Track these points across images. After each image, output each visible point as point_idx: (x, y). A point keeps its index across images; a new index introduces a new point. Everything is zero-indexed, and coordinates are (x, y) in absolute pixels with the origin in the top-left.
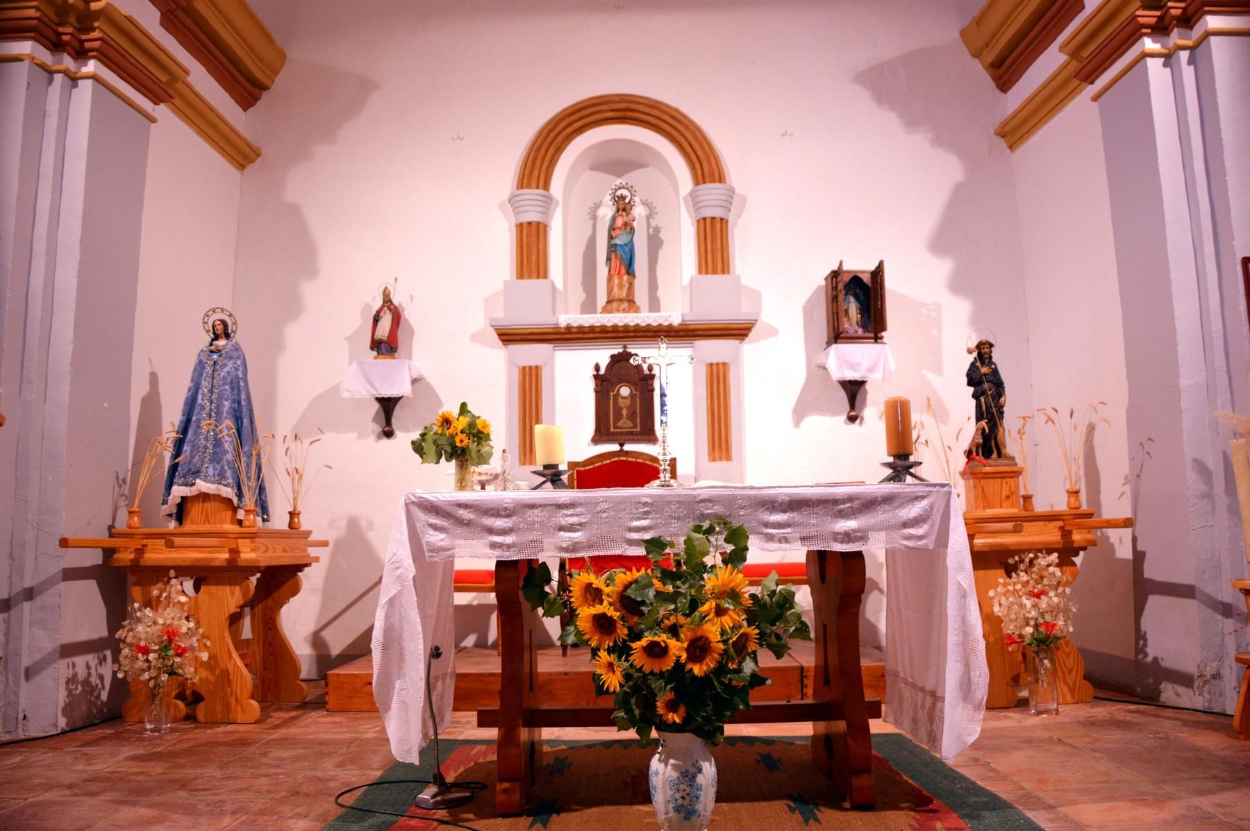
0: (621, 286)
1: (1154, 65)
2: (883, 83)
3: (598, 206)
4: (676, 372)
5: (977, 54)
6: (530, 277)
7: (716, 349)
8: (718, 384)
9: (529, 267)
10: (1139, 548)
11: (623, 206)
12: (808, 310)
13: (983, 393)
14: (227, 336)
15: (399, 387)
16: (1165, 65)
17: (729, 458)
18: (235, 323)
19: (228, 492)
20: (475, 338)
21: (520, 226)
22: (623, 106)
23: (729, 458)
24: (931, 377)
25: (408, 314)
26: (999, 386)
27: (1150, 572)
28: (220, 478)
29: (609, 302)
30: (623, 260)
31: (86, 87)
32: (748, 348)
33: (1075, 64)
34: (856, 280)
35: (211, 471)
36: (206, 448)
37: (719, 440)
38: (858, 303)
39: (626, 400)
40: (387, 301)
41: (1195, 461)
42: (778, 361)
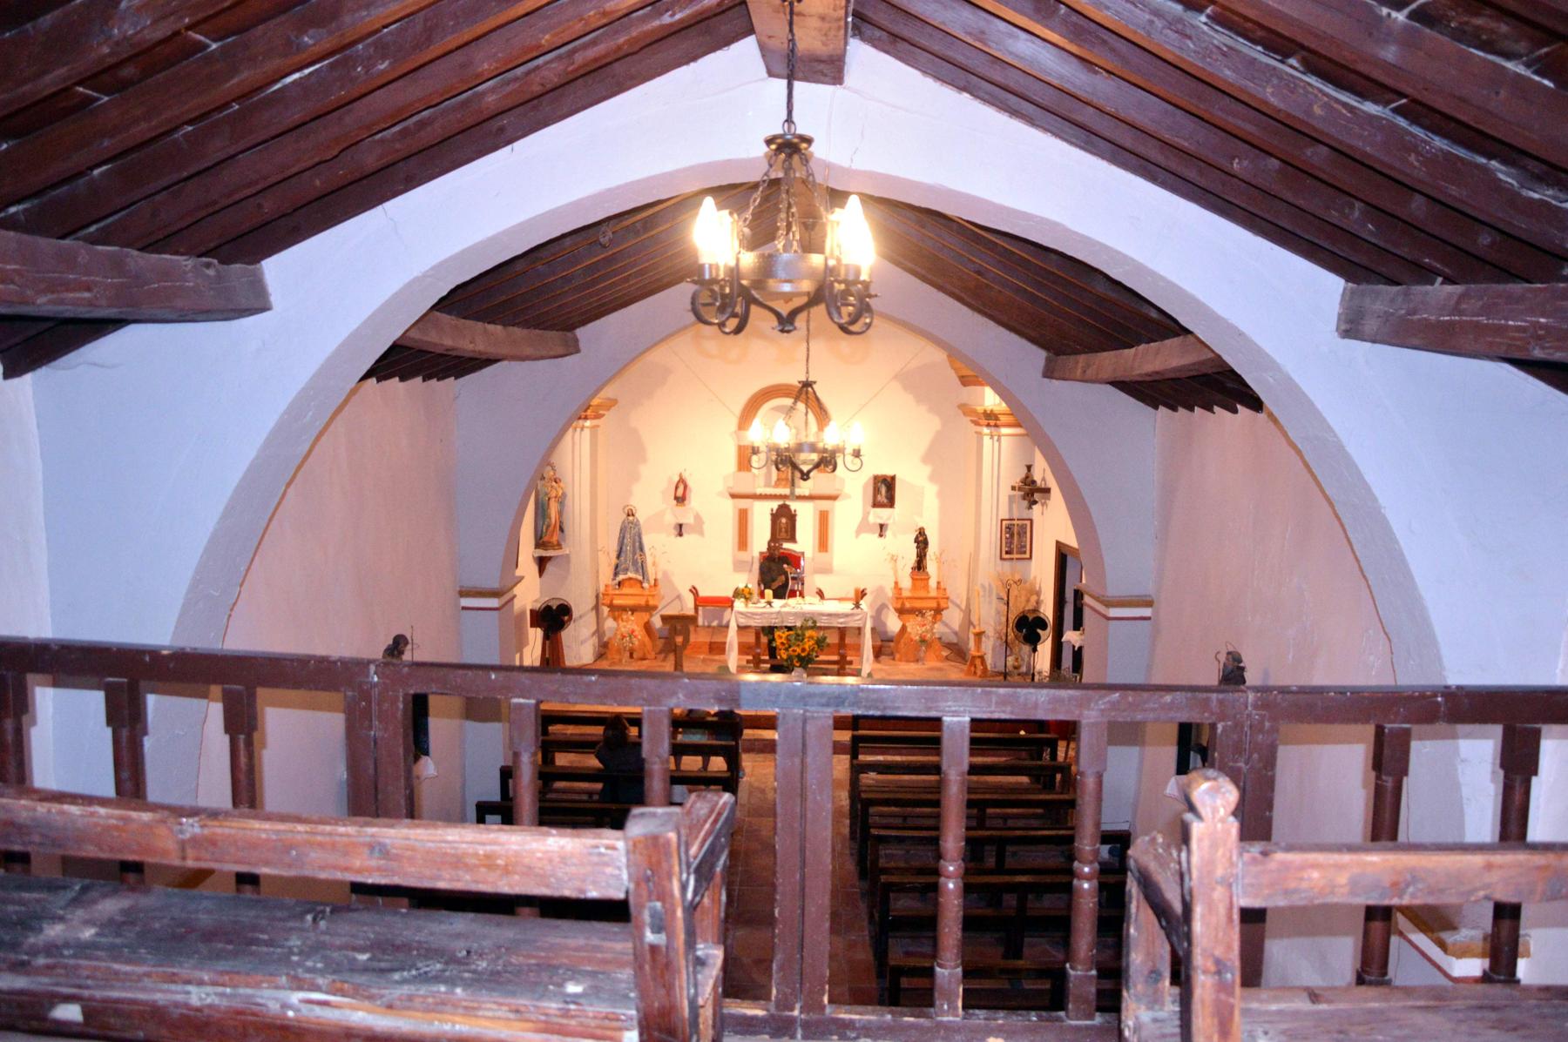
2: (912, 382)
4: (805, 514)
7: (824, 505)
8: (824, 520)
12: (865, 487)
15: (688, 520)
20: (720, 494)
25: (690, 483)
28: (637, 571)
31: (587, 432)
32: (837, 503)
37: (823, 543)
38: (885, 490)
39: (784, 523)
42: (851, 507)
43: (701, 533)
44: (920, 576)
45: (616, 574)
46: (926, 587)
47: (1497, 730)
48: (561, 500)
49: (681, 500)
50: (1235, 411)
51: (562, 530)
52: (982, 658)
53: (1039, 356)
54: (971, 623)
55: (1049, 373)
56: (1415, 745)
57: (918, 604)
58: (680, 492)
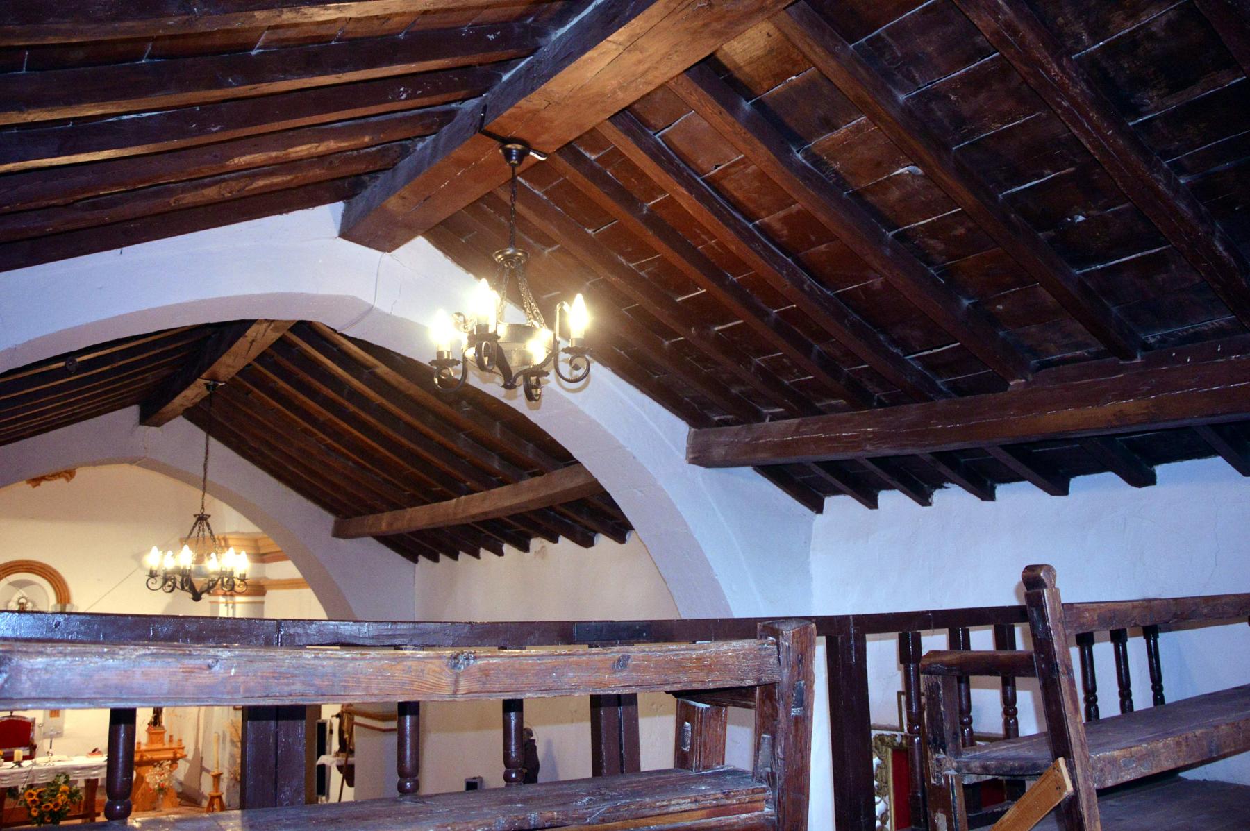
44: (157, 730)
46: (162, 741)
47: (947, 630)
50: (500, 553)
52: (220, 797)
53: (329, 519)
54: (203, 769)
55: (339, 532)
56: (923, 638)
57: (156, 756)
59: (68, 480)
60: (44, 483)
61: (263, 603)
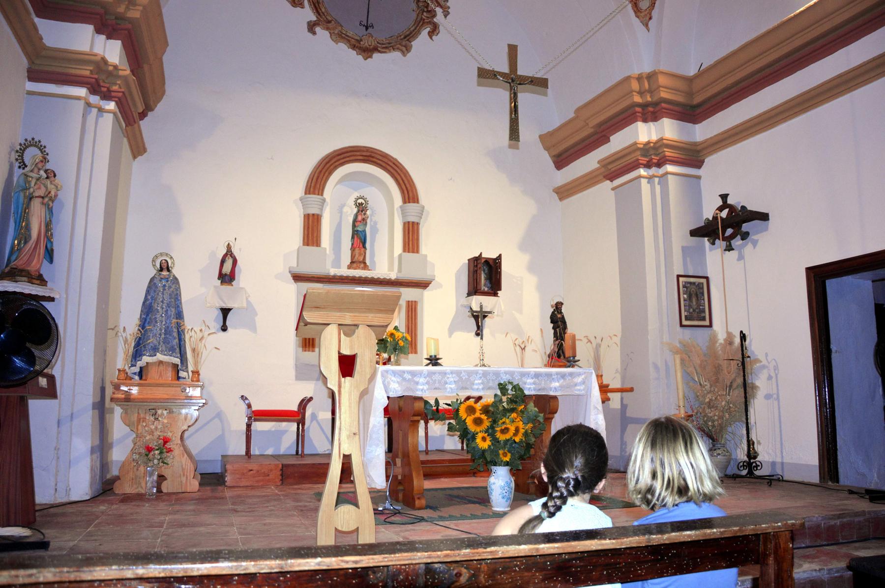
0: (360, 254)
1: (644, 181)
3: (342, 206)
5: (547, 148)
6: (313, 245)
9: (313, 239)
10: (625, 402)
11: (362, 208)
13: (558, 327)
14: (168, 270)
16: (648, 182)
17: (416, 352)
18: (173, 263)
19: (177, 361)
21: (307, 217)
22: (368, 154)
23: (416, 352)
24: (517, 315)
26: (564, 323)
27: (629, 414)
29: (352, 262)
30: (359, 239)
32: (427, 293)
33: (603, 170)
34: (487, 262)
35: (164, 348)
36: (160, 335)
38: (485, 275)
40: (229, 253)
41: (654, 363)
43: (253, 328)
45: (137, 355)
48: (50, 201)
49: (227, 278)
51: (50, 255)
58: (227, 268)
59: (404, 55)
60: (376, 55)
61: (699, 177)
